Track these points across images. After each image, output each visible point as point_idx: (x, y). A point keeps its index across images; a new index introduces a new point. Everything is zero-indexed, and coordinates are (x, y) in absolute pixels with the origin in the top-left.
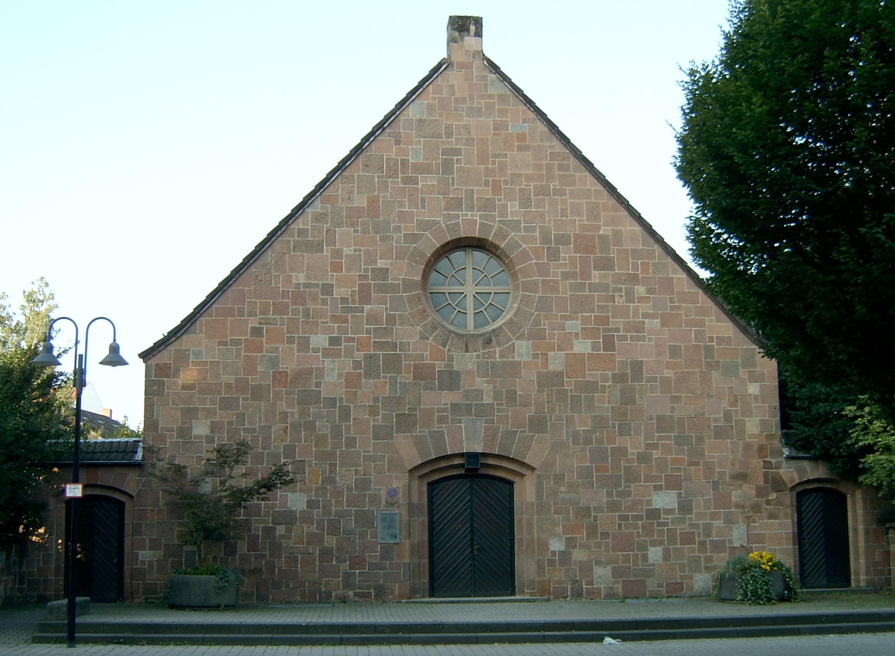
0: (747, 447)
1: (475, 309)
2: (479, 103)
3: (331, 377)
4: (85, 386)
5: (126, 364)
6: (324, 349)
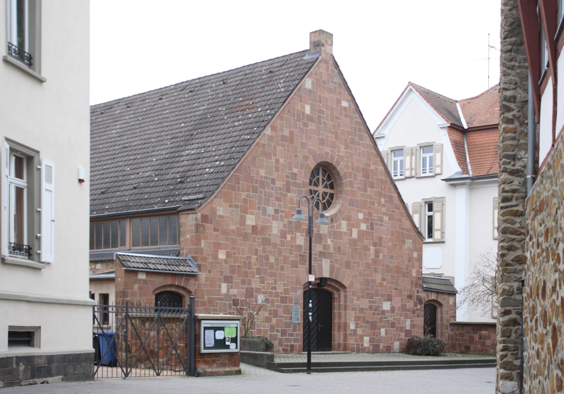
0: (412, 282)
1: (314, 190)
2: (331, 86)
3: (275, 231)
4: (308, 373)
5: (41, 81)
6: (273, 215)
